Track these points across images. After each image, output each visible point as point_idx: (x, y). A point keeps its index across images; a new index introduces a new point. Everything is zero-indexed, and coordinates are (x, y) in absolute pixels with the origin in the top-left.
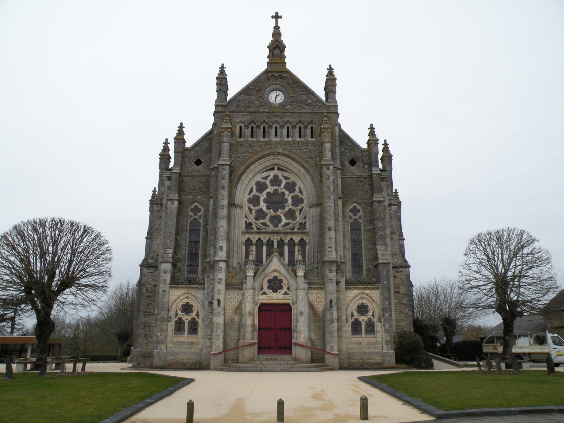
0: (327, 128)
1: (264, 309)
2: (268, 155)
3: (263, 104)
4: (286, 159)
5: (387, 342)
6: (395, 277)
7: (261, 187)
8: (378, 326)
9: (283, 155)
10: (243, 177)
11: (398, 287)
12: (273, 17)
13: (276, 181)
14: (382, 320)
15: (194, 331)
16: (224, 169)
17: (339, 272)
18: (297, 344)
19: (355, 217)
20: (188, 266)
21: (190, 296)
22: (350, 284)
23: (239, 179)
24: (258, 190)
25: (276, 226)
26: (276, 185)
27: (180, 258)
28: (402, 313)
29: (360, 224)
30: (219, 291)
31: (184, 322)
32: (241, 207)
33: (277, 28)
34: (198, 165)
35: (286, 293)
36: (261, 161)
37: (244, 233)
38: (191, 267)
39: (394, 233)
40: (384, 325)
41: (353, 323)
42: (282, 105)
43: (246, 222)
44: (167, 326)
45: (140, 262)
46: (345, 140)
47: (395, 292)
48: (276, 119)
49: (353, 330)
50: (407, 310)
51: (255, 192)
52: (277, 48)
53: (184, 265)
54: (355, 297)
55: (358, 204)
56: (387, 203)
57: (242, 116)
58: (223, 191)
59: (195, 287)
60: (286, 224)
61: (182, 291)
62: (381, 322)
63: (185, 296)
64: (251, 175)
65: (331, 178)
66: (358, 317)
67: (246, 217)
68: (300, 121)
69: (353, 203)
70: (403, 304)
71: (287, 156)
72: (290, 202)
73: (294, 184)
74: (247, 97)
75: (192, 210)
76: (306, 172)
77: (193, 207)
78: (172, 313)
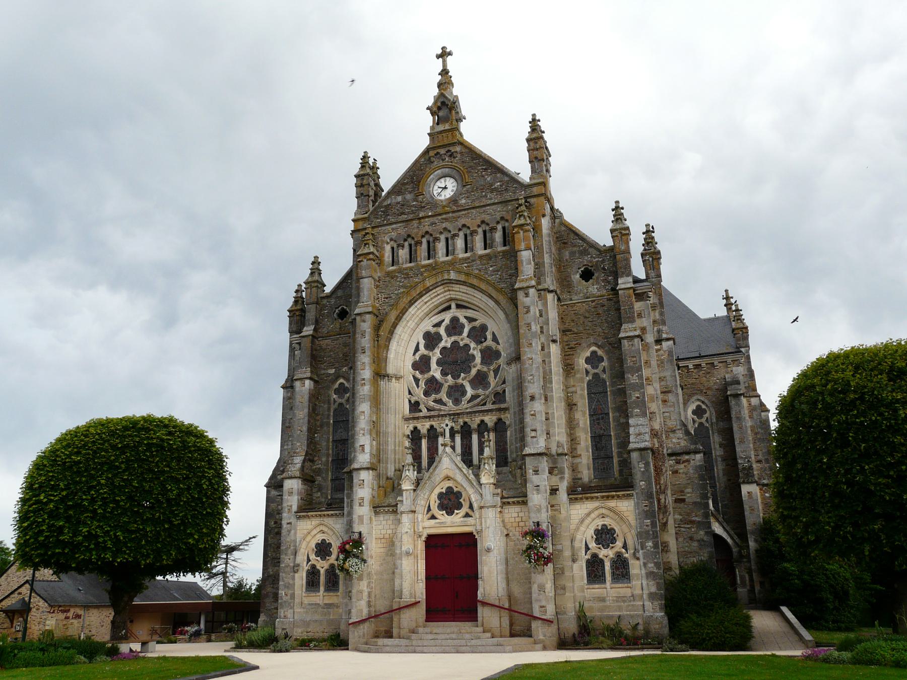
0: (523, 225)
1: (434, 543)
2: (435, 286)
3: (423, 205)
4: (464, 288)
5: (652, 596)
6: (675, 472)
7: (431, 340)
8: (636, 567)
9: (458, 282)
10: (399, 330)
11: (682, 491)
12: (438, 57)
13: (455, 327)
14: (640, 554)
15: (334, 585)
16: (364, 321)
17: (556, 472)
18: (484, 604)
19: (596, 371)
20: (332, 480)
21: (325, 529)
22: (578, 491)
23: (392, 332)
24: (427, 347)
25: (457, 402)
26: (455, 334)
27: (319, 468)
28: (691, 539)
29: (604, 381)
30: (361, 518)
31: (319, 571)
32: (398, 378)
33: (445, 72)
34: (587, 281)
35: (467, 515)
36: (425, 298)
37: (407, 419)
38: (337, 482)
39: (669, 392)
40: (645, 564)
41: (588, 561)
42: (453, 200)
43: (410, 401)
44: (293, 578)
45: (266, 480)
46: (568, 236)
47: (677, 501)
48: (444, 225)
49: (589, 575)
50: (702, 533)
51: (423, 350)
52: (445, 109)
53: (325, 479)
54: (588, 515)
55: (599, 347)
56: (650, 338)
57: (393, 229)
58: (362, 356)
59: (332, 515)
60: (474, 397)
61: (315, 521)
62: (638, 559)
63: (318, 529)
64: (412, 324)
65: (535, 311)
66: (597, 551)
67: (410, 393)
68: (483, 222)
69: (589, 346)
70: (692, 522)
71: (464, 283)
72: (478, 360)
73: (484, 328)
74: (399, 199)
75: (337, 391)
76: (496, 306)
77: (336, 386)
78: (301, 558)
